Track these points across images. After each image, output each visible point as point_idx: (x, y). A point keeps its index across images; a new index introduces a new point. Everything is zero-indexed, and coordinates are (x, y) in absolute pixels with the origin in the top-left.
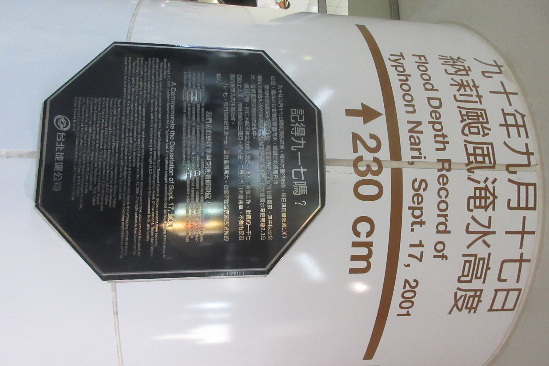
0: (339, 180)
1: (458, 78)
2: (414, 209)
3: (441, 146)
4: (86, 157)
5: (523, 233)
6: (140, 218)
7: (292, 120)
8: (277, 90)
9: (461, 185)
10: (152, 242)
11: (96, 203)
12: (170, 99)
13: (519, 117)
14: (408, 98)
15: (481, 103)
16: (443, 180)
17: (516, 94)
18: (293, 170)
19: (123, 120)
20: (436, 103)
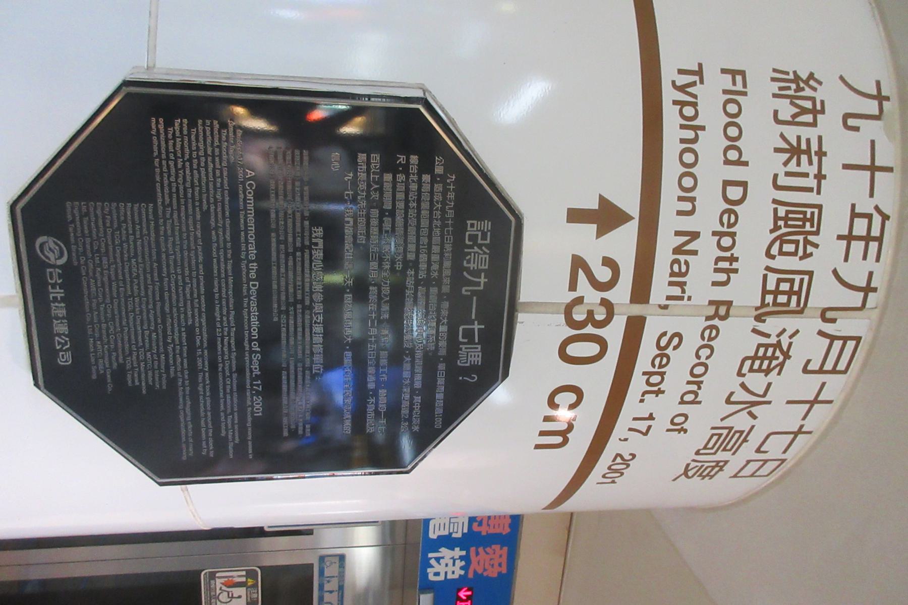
0: (535, 339)
3: (723, 277)
6: (208, 404)
7: (467, 242)
8: (445, 184)
9: (738, 338)
10: (230, 437)
11: (133, 382)
13: (877, 220)
15: (819, 193)
16: (710, 334)
17: (890, 170)
18: (461, 329)
19: (163, 245)
20: (735, 193)
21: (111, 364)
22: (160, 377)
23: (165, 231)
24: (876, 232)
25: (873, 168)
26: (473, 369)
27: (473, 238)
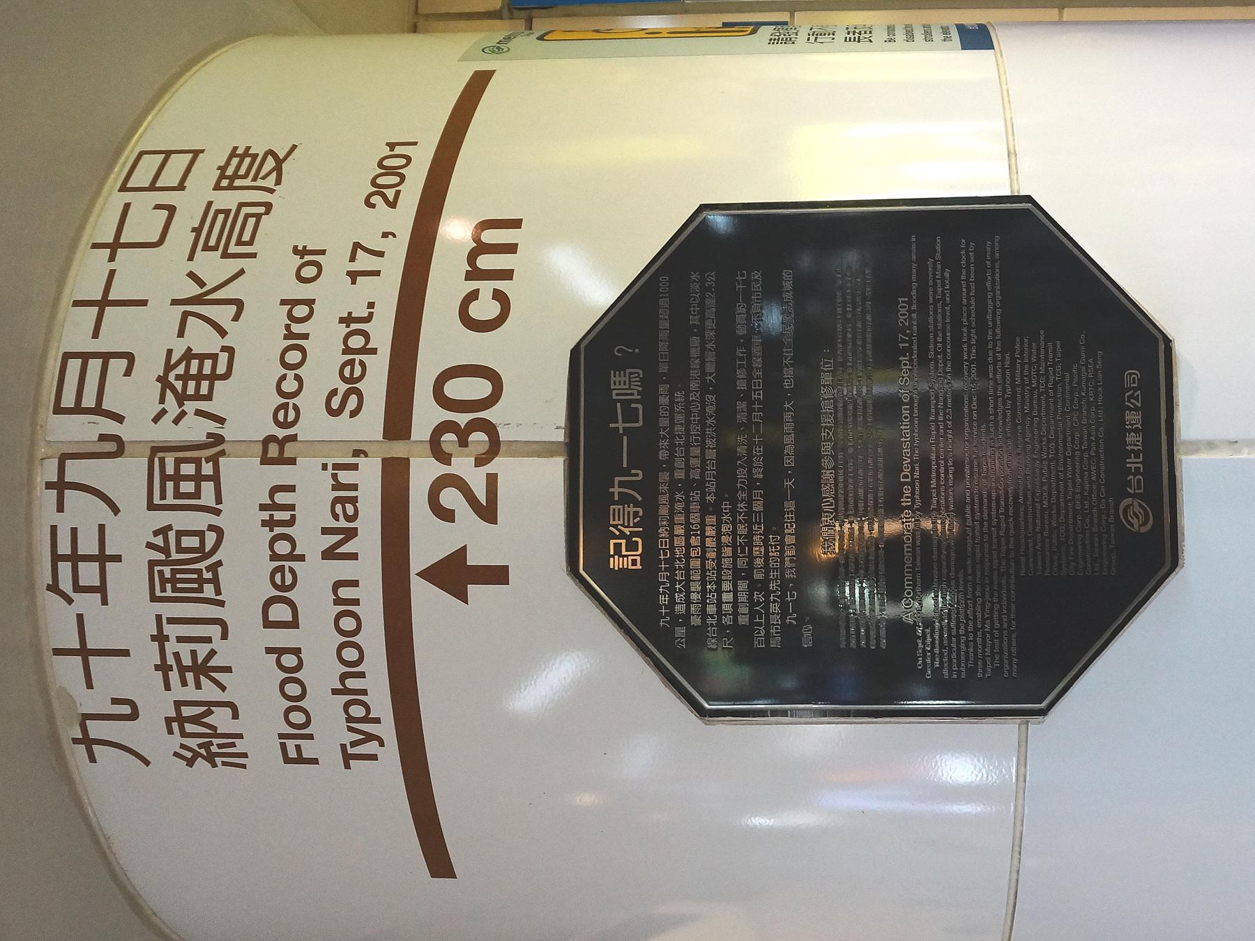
0: (537, 404)
1: (209, 692)
2: (364, 350)
3: (281, 498)
5: (103, 303)
9: (245, 406)
10: (939, 266)
11: (1055, 346)
12: (914, 580)
13: (66, 584)
14: (348, 624)
15: (159, 618)
16: (286, 414)
17: (57, 652)
20: (280, 612)
22: (1022, 353)
23: (1008, 543)
24: (65, 568)
25: (84, 652)
26: (621, 365)
27: (632, 546)
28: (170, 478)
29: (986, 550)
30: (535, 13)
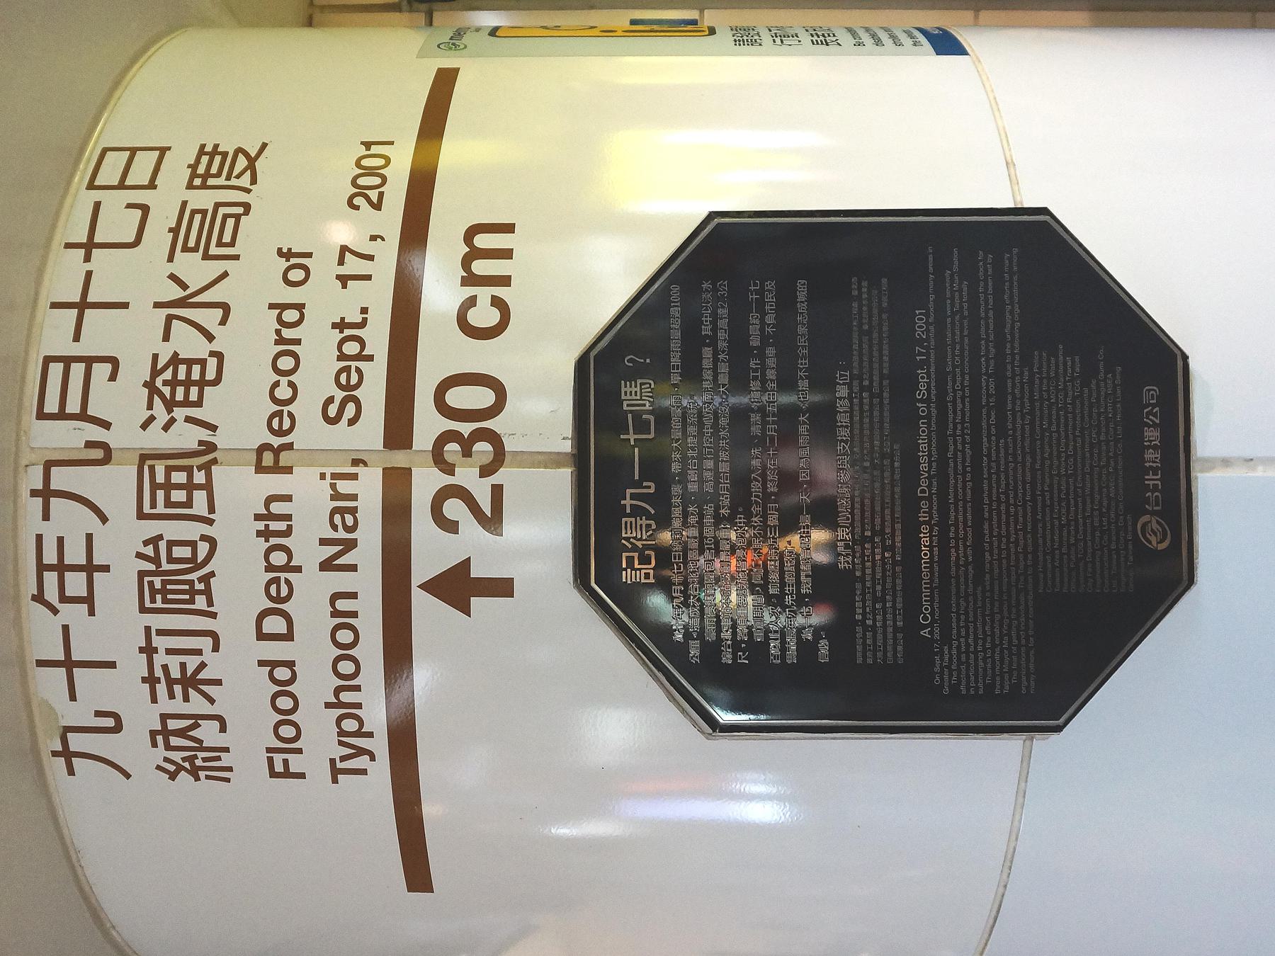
0: (542, 411)
1: (197, 704)
4: (1100, 460)
5: (83, 305)
9: (237, 412)
13: (52, 594)
14: (345, 636)
15: (148, 629)
17: (41, 663)
20: (275, 625)
21: (1098, 386)
22: (1040, 368)
23: (1026, 559)
24: (51, 578)
25: (69, 664)
27: (645, 560)
28: (160, 486)
29: (1004, 566)
30: (436, 6)
